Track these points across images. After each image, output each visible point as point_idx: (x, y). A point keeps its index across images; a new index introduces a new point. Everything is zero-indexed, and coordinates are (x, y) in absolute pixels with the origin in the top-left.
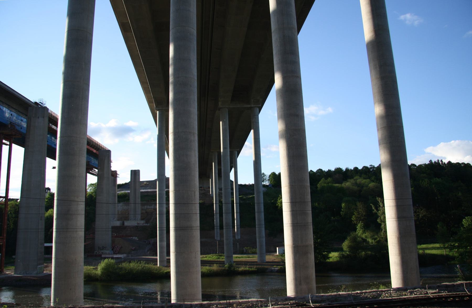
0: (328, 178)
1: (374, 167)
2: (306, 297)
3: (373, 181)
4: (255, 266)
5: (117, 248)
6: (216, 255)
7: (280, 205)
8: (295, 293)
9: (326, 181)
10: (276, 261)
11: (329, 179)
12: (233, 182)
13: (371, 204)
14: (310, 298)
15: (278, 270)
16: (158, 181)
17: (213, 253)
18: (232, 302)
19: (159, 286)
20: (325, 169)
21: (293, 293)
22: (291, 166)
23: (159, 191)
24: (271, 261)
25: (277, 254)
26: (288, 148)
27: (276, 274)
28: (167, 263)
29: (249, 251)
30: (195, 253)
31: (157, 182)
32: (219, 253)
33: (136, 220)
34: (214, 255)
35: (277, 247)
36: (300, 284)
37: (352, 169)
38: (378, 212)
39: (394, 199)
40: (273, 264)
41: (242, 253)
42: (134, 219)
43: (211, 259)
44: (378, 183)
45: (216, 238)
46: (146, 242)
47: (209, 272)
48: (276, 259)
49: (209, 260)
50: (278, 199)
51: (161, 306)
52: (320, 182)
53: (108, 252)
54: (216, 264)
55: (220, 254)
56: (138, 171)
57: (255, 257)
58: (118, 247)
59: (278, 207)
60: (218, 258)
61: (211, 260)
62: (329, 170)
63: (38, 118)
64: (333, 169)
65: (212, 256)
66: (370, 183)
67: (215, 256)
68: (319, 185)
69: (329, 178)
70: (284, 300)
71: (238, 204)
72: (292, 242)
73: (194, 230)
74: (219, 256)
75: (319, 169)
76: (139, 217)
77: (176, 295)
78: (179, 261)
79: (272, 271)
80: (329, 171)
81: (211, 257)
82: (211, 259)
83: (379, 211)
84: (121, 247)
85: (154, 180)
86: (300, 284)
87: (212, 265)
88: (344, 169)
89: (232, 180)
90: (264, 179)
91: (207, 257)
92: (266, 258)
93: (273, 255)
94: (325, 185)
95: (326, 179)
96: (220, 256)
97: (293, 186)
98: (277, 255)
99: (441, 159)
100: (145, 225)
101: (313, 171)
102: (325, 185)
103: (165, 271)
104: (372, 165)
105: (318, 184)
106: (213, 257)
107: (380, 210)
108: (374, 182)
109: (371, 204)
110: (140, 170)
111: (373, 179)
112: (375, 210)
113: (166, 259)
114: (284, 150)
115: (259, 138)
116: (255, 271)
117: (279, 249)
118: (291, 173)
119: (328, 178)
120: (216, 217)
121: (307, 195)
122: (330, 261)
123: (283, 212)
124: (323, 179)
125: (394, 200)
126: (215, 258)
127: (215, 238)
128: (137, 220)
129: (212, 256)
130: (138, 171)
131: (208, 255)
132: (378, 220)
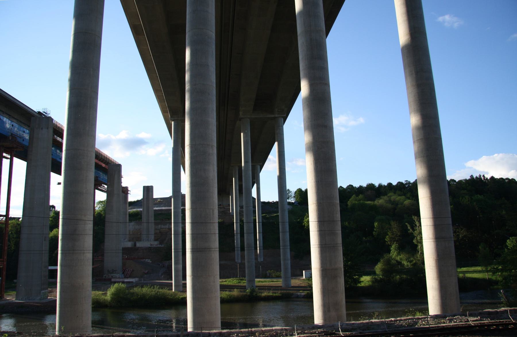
0: (360, 195)
1: (410, 182)
2: (335, 325)
3: (409, 198)
4: (279, 291)
5: (128, 272)
6: (237, 278)
7: (307, 225)
8: (323, 320)
9: (357, 198)
10: (302, 285)
11: (361, 196)
12: (255, 199)
13: (406, 224)
14: (340, 326)
15: (305, 295)
16: (173, 198)
17: (233, 277)
18: (254, 330)
19: (174, 313)
20: (356, 185)
21: (321, 320)
22: (318, 181)
23: (174, 209)
24: (297, 285)
25: (303, 278)
26: (315, 162)
27: (303, 299)
28: (183, 288)
29: (273, 275)
30: (214, 277)
31: (172, 199)
32: (240, 277)
33: (149, 241)
34: (234, 279)
35: (304, 270)
36: (329, 311)
37: (386, 185)
38: (414, 232)
39: (432, 217)
40: (299, 289)
41: (265, 277)
42: (147, 240)
43: (231, 283)
44: (415, 200)
45: (236, 261)
46: (160, 264)
47: (229, 298)
48: (302, 284)
49: (229, 284)
50: (305, 218)
51: (177, 335)
52: (350, 200)
53: (118, 276)
54: (237, 288)
55: (241, 278)
56: (152, 187)
57: (279, 281)
58: (129, 270)
59: (305, 227)
60: (239, 283)
61: (231, 285)
62: (360, 186)
63: (42, 129)
64: (365, 185)
65: (232, 280)
66: (405, 201)
67: (235, 280)
68: (350, 202)
69: (360, 195)
70: (311, 329)
71: (261, 224)
72: (320, 264)
73: (212, 252)
74: (240, 281)
75: (350, 185)
76: (152, 237)
77: (192, 323)
78: (196, 285)
79: (298, 297)
80: (361, 187)
81: (231, 281)
82: (231, 283)
83: (415, 230)
84: (133, 271)
85: (169, 197)
86: (329, 311)
87: (232, 290)
88: (377, 185)
89: (254, 197)
90: (289, 196)
91: (226, 282)
92: (292, 282)
93: (299, 279)
94: (357, 202)
95: (357, 196)
96: (241, 280)
97: (321, 203)
98: (303, 279)
99: (483, 174)
100: (159, 246)
101: (343, 187)
102: (357, 202)
103: (181, 297)
104: (407, 181)
105: (349, 202)
106: (233, 281)
107: (416, 230)
108: (410, 199)
109: (406, 224)
110: (153, 186)
111: (408, 196)
112: (411, 230)
113: (182, 284)
114: (311, 164)
115: (284, 152)
116: (280, 296)
117: (306, 272)
118: (318, 190)
119: (359, 195)
120: (236, 238)
121: (336, 214)
122: (361, 285)
123: (310, 232)
124: (354, 195)
125: (432, 219)
126: (236, 282)
127: (235, 261)
128: (150, 241)
129: (232, 280)
130: (152, 187)
131: (227, 279)
132: (415, 241)
